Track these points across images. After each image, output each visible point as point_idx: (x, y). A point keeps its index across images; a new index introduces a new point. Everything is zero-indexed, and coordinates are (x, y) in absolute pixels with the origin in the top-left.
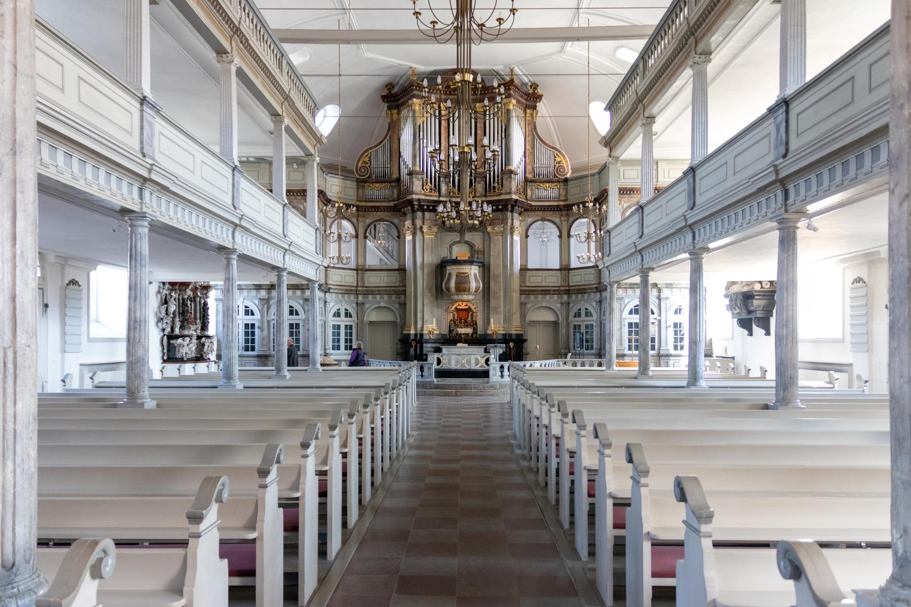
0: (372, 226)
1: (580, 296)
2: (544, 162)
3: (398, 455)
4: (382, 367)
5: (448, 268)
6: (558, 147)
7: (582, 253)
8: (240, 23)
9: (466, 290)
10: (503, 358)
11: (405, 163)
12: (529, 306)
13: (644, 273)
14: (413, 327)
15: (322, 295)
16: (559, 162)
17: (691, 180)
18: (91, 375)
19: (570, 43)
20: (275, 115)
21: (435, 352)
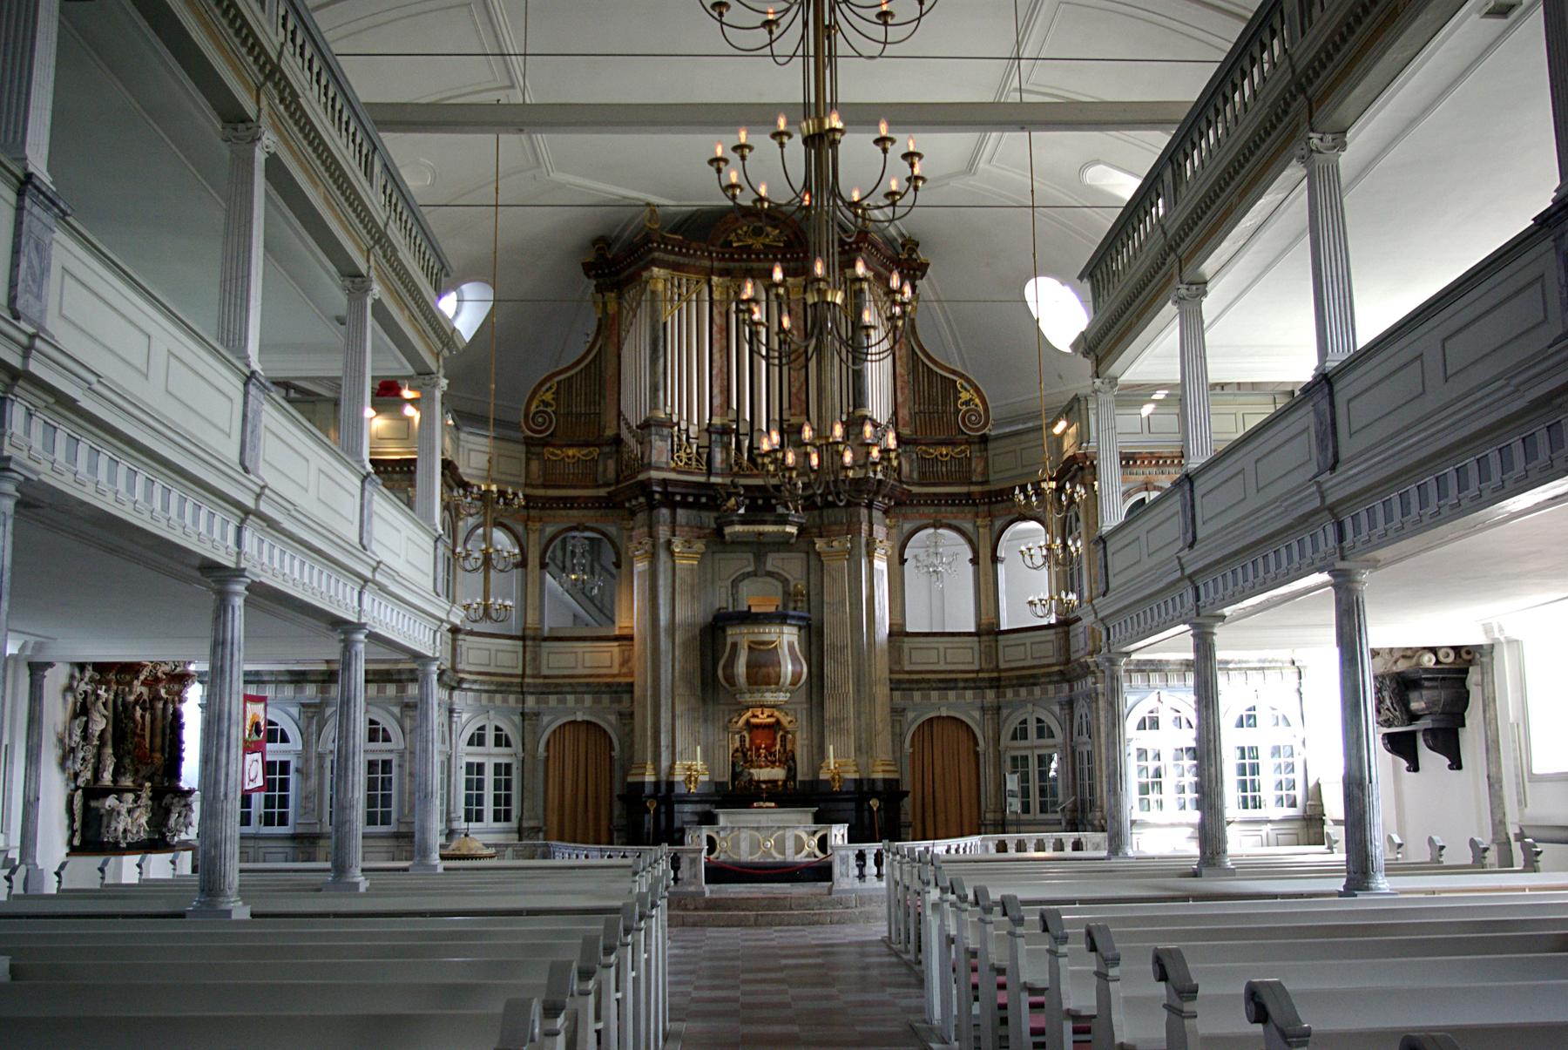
0: (558, 541)
1: (1023, 691)
5: (729, 631)
7: (1027, 588)
14: (649, 766)
15: (444, 694)
17: (1324, 405)
18: (6, 872)
20: (354, 280)
21: (700, 823)
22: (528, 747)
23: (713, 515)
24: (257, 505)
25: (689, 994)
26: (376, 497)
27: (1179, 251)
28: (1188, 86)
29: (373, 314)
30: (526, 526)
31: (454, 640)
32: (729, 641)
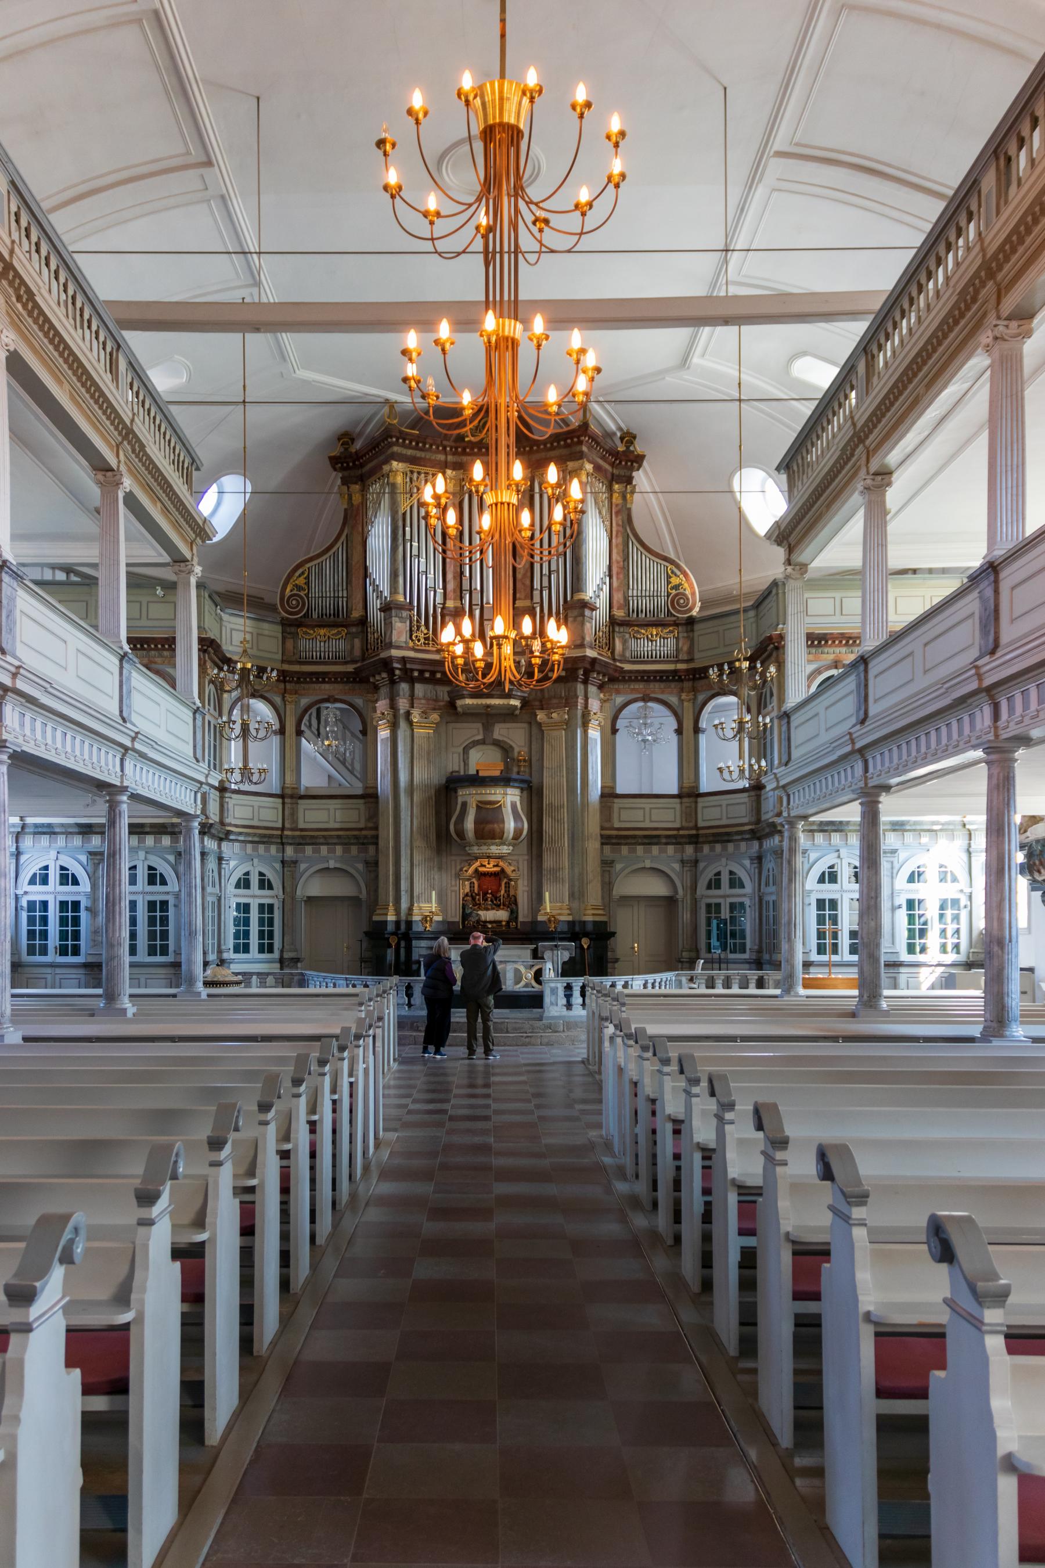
0: (314, 710)
1: (718, 847)
2: (648, 584)
3: (353, 1196)
4: (331, 990)
5: (460, 792)
6: (672, 556)
7: (724, 760)
8: (12, 252)
9: (497, 836)
10: (569, 969)
11: (376, 588)
12: (619, 866)
13: (870, 798)
14: (391, 908)
16: (676, 587)
17: (989, 592)
19: (707, 330)
20: (101, 467)
22: (288, 889)
23: (447, 689)
24: (14, 683)
25: (406, 1106)
26: (134, 674)
27: (868, 442)
28: (883, 276)
29: (125, 503)
30: (284, 697)
31: (222, 798)
32: (460, 800)
